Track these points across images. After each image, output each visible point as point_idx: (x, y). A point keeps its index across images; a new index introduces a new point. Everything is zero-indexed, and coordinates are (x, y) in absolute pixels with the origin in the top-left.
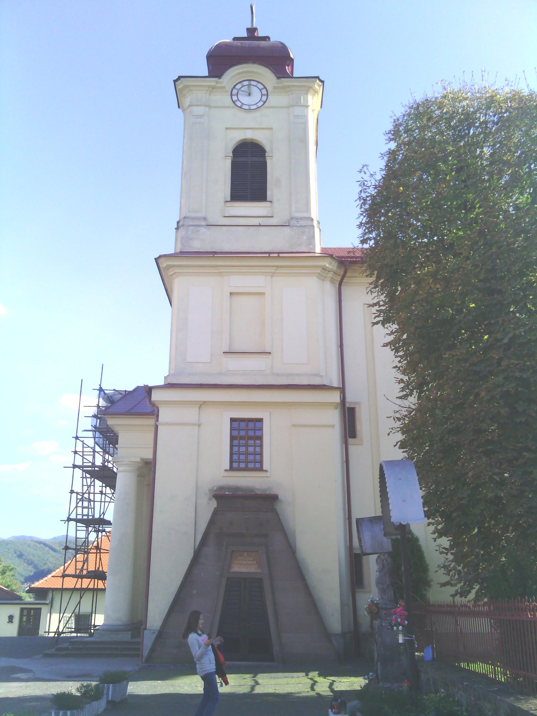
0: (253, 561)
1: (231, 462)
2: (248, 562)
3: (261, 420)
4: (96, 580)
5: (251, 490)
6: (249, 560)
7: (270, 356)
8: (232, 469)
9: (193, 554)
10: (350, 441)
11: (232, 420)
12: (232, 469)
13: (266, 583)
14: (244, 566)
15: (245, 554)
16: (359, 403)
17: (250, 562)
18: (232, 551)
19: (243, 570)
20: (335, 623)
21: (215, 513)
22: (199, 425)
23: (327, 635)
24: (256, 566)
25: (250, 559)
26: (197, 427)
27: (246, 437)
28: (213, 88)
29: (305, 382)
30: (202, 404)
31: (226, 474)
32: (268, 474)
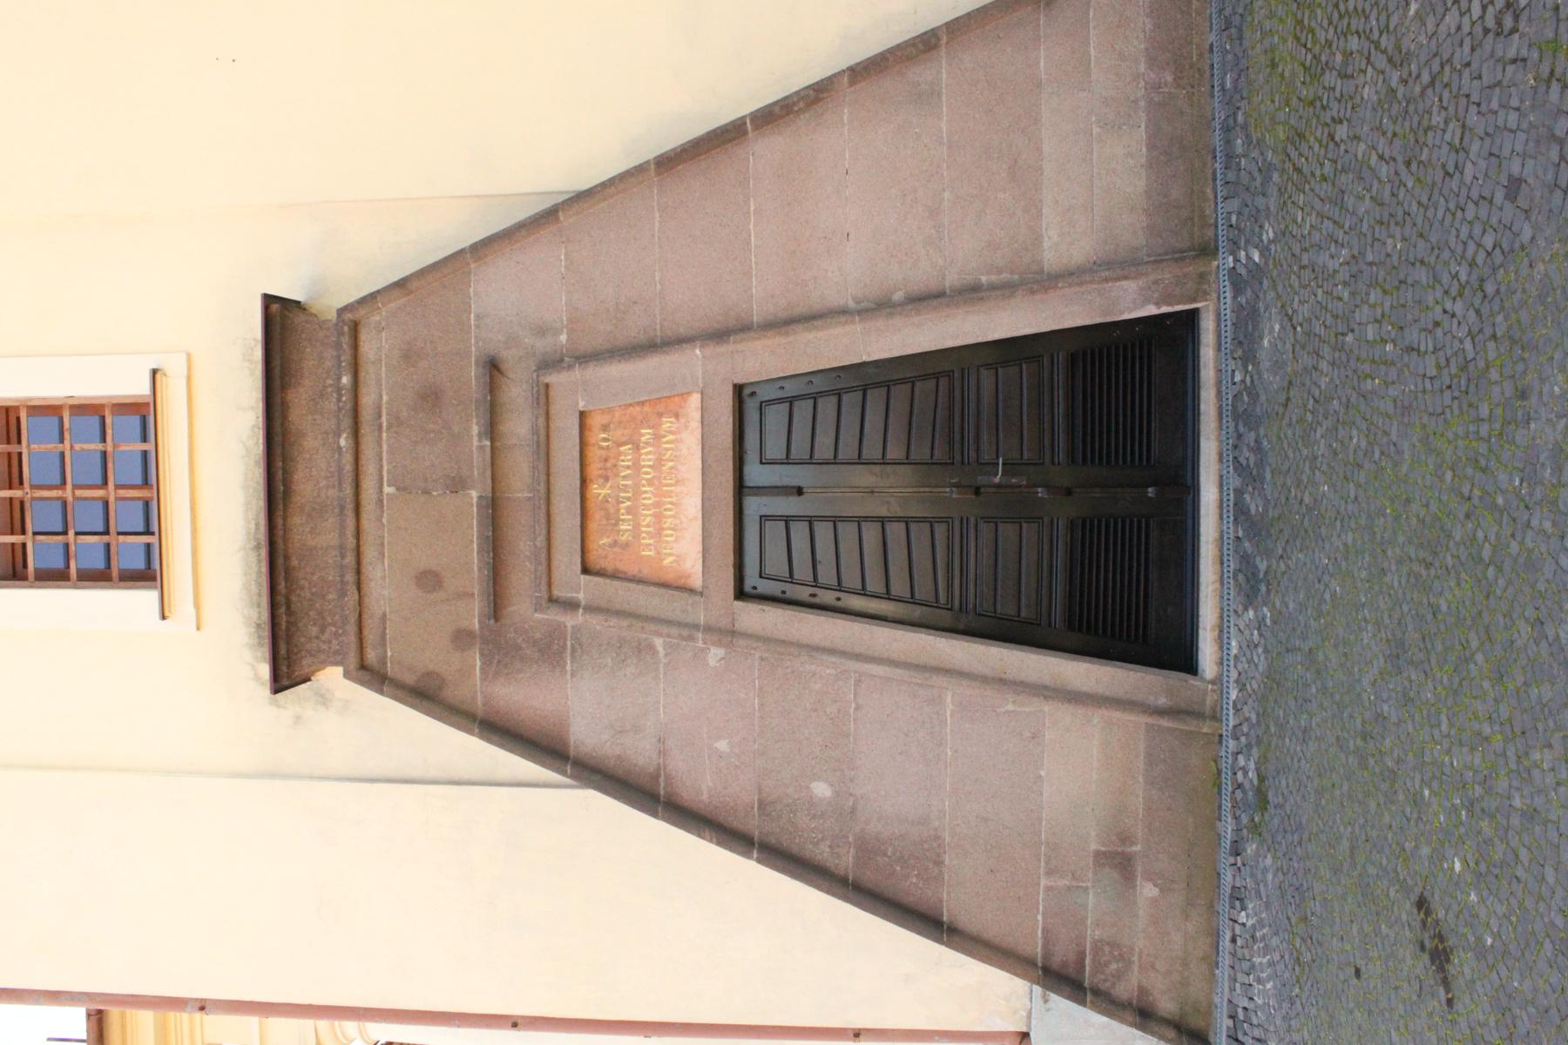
0: (637, 448)
6: (636, 466)
13: (763, 360)
14: (667, 498)
15: (598, 490)
17: (648, 458)
18: (586, 570)
21: (373, 675)
24: (667, 423)
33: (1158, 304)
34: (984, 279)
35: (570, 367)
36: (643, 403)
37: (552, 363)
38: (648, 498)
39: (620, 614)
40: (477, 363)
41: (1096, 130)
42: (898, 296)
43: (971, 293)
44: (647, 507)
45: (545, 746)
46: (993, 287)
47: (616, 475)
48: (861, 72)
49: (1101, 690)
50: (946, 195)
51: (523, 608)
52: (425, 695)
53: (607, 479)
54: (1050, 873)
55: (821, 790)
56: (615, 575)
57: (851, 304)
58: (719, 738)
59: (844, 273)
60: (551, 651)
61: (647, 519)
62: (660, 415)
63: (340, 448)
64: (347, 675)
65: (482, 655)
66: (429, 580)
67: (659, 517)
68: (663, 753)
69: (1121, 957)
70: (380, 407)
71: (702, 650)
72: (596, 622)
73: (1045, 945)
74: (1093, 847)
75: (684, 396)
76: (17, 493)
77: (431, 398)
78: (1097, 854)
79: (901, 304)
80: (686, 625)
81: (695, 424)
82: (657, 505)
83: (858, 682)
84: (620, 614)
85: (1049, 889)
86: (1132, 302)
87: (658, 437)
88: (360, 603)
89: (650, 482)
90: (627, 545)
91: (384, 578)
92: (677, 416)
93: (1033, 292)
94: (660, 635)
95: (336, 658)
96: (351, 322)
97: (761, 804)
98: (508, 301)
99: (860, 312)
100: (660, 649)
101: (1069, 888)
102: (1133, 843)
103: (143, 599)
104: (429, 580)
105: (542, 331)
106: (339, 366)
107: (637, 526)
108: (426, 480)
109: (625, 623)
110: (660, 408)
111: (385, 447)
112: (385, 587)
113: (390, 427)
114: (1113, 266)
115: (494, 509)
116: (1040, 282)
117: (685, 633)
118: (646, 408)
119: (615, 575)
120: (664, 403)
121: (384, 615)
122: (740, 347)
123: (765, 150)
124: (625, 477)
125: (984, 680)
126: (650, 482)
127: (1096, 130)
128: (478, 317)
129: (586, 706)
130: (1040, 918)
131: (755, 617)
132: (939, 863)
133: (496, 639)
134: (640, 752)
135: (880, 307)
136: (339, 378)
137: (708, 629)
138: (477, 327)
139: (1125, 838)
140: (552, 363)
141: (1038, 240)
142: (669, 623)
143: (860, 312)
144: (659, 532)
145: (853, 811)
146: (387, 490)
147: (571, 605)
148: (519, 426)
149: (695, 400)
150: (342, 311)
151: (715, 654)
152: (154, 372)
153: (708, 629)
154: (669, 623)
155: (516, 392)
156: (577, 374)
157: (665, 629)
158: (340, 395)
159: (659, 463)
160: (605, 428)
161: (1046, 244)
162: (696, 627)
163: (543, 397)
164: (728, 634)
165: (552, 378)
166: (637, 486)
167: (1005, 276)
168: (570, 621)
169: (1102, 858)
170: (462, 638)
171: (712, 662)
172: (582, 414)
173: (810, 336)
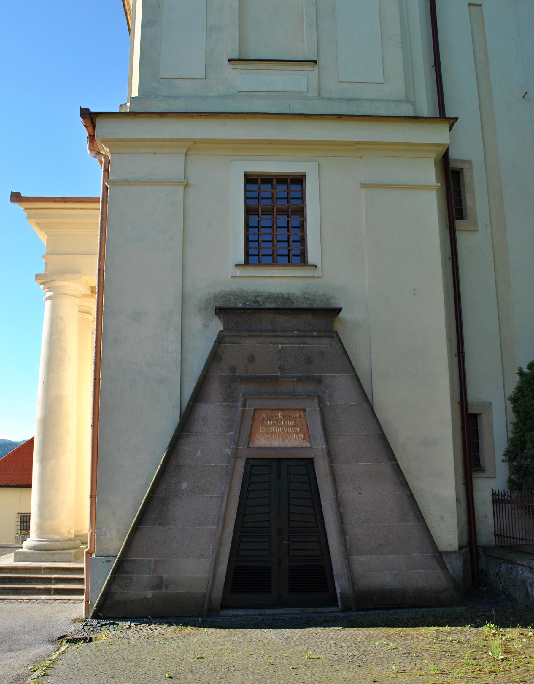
0: (294, 426)
1: (247, 254)
2: (286, 430)
3: (299, 180)
4: (498, 504)
5: (288, 299)
6: (288, 426)
7: (316, 68)
8: (247, 263)
9: (179, 420)
10: (459, 224)
11: (250, 179)
12: (247, 263)
13: (322, 468)
14: (280, 436)
15: (280, 414)
16: (470, 162)
17: (290, 430)
18: (255, 410)
19: (276, 444)
20: (448, 533)
21: (220, 340)
22: (186, 186)
23: (440, 556)
24: (302, 436)
25: (290, 423)
26: (181, 188)
27: (275, 213)
28: (195, 143)
29: (383, 113)
30: (191, 147)
31: (238, 272)
32: (318, 273)
33: (340, 593)
34: (347, 537)
35: (320, 406)
36: (308, 428)
37: (321, 401)
38: (278, 430)
39: (242, 422)
40: (320, 376)
41: (394, 572)
42: (342, 510)
43: (343, 532)
44: (275, 429)
45: (198, 396)
46: (345, 540)
47: (285, 420)
48: (411, 496)
49: (479, 526)
50: (374, 525)
51: (242, 388)
52: (215, 357)
53: (284, 417)
54: (155, 561)
55: (184, 485)
56: (253, 419)
57: (339, 495)
58: (201, 452)
59: (350, 494)
60: (229, 398)
61: (272, 429)
62: (304, 434)
63: (294, 331)
64: (221, 331)
65: (228, 375)
66: (251, 359)
67: (272, 433)
68: (196, 434)
69: (126, 586)
70: (306, 344)
71: (230, 447)
72: (239, 413)
73: (133, 561)
74: (165, 576)
75: (310, 442)
76: (275, 210)
77: (309, 361)
78: (162, 577)
79: (339, 511)
80: (238, 442)
81: (301, 445)
82: (276, 433)
83: (220, 497)
84: (242, 422)
85: (150, 561)
86: (340, 585)
87: (297, 433)
88: (246, 337)
89: (283, 431)
90: (263, 423)
91: (252, 344)
92: (304, 439)
93: (344, 552)
94: (235, 434)
95: (226, 328)
96: (334, 335)
97: (180, 466)
98: (341, 389)
99: (337, 497)
100: (230, 434)
101: (150, 568)
102: (166, 589)
103: (241, 259)
104: (251, 359)
105: (330, 397)
106: (319, 331)
107: (269, 426)
108: (283, 358)
109: (239, 423)
110: (306, 434)
111: (293, 345)
112: (250, 344)
113: (300, 347)
114: (352, 580)
115: (275, 379)
116: (347, 554)
117: (236, 442)
118: (306, 430)
119: (253, 419)
120: (308, 436)
121: (240, 344)
122: (326, 460)
123: (386, 468)
124: (284, 422)
125: (221, 538)
126: (283, 431)
127: (394, 572)
128: (335, 376)
129: (212, 411)
130: (140, 558)
131: (241, 465)
132: (160, 524)
133: (233, 380)
134: (197, 426)
135: (338, 504)
136: (315, 331)
137: (237, 449)
138: (331, 376)
139: (167, 586)
140: (321, 401)
141: (360, 554)
142: (239, 436)
143: (337, 497)
144: (267, 433)
145: (177, 496)
146: (280, 346)
147: (244, 405)
148: (300, 388)
149: (308, 445)
150: (336, 332)
151: (228, 451)
152: (316, 266)
153: (237, 449)
154: (239, 436)
155: (311, 387)
156: (317, 408)
157: (237, 435)
158: (309, 331)
159: (288, 433)
160: (300, 416)
161: (359, 557)
162: (237, 446)
163: (310, 396)
164: (235, 455)
165: (316, 401)
166: (281, 426)
167: (348, 544)
168: (240, 404)
169: (161, 579)
170: (233, 369)
171: (226, 450)
172: (304, 410)
173: (329, 481)
